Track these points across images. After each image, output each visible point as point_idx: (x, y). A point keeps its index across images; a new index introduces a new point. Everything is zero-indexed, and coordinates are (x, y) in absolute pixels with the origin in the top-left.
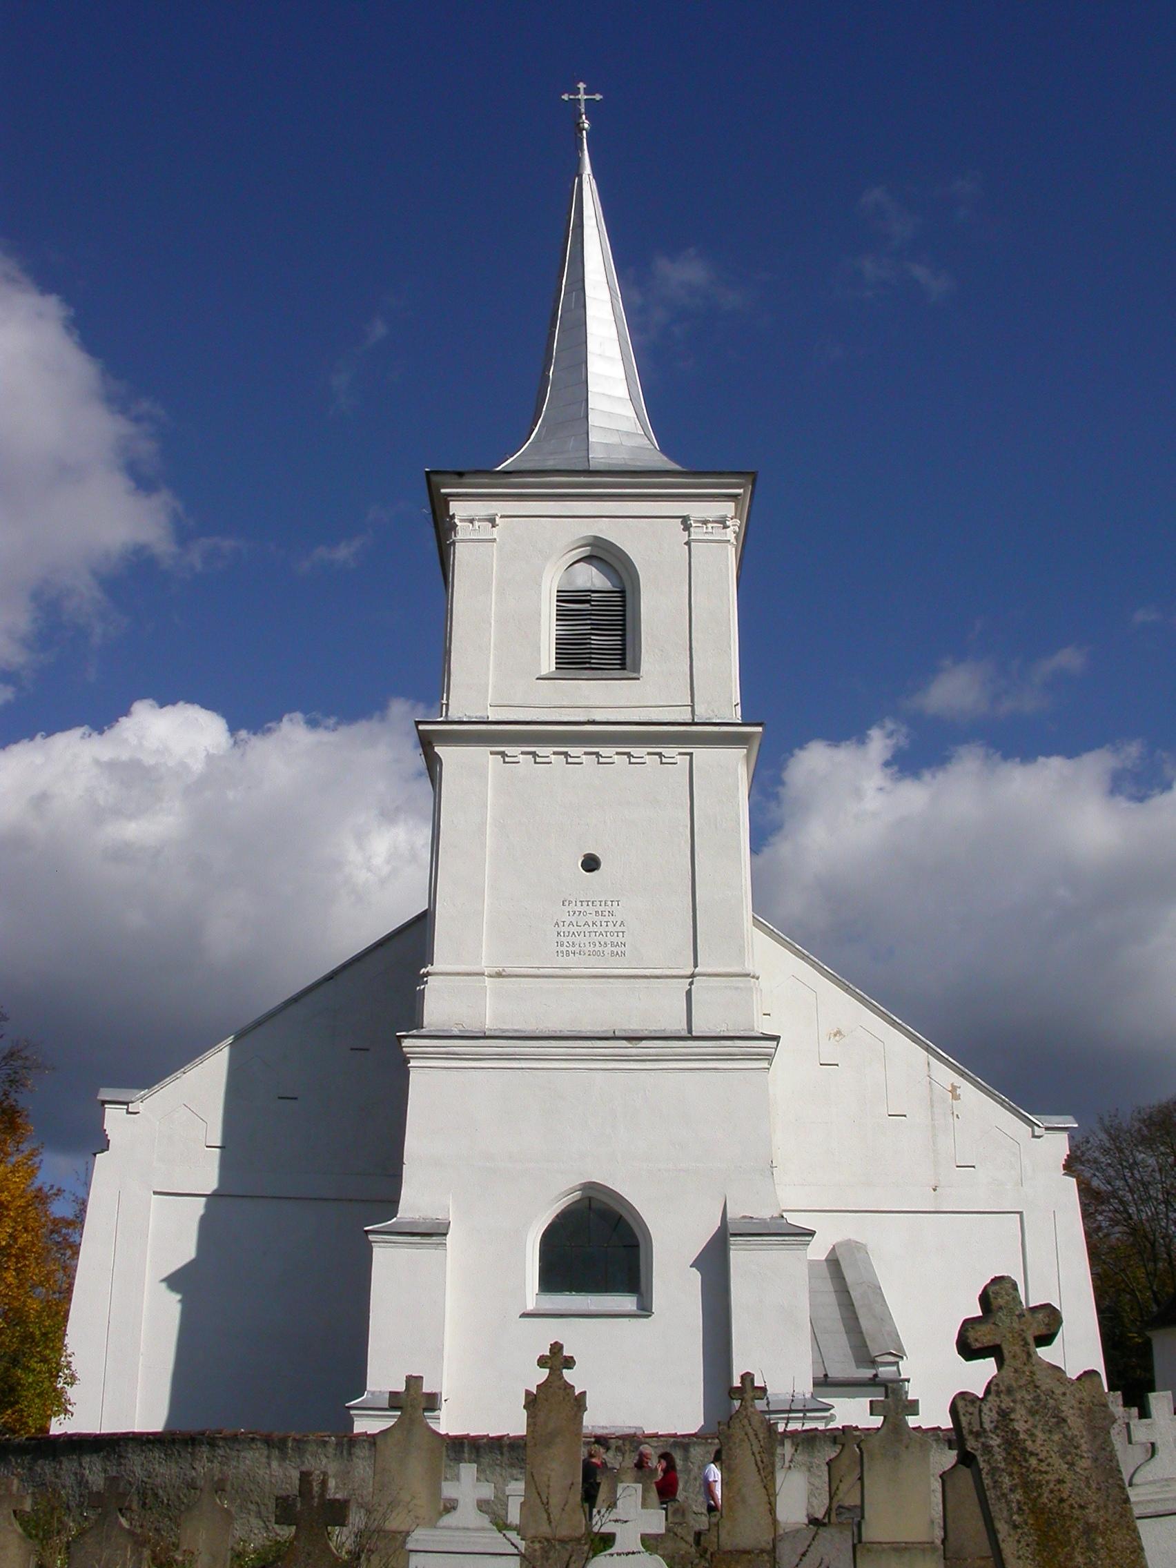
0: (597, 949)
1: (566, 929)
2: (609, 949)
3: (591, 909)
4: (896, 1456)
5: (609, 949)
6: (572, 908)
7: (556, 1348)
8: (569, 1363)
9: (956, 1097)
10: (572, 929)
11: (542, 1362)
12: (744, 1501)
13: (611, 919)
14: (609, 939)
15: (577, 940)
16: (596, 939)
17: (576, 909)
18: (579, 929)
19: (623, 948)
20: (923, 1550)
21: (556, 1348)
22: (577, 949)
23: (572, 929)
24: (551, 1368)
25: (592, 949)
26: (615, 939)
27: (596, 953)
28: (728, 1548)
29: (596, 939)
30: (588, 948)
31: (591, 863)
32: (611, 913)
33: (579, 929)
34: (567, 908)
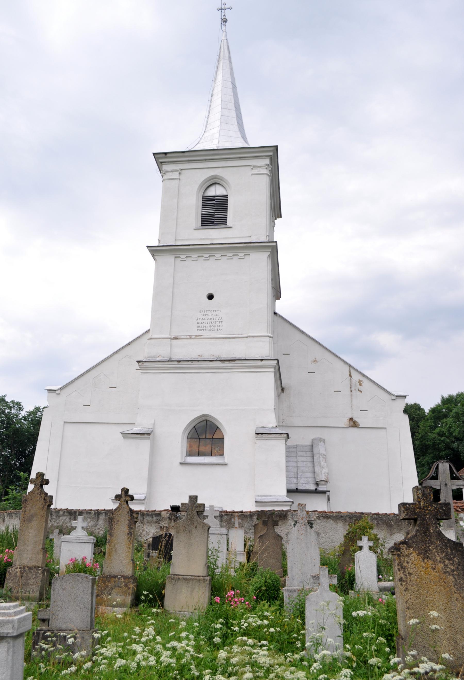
0: (212, 328)
1: (201, 321)
2: (216, 328)
3: (210, 313)
4: (190, 531)
5: (216, 328)
6: (203, 313)
7: (125, 491)
8: (47, 482)
9: (361, 385)
10: (203, 321)
11: (118, 497)
12: (116, 551)
13: (217, 317)
14: (216, 324)
15: (204, 325)
16: (212, 324)
17: (205, 314)
18: (205, 321)
19: (221, 328)
20: (199, 580)
21: (125, 491)
22: (204, 328)
23: (203, 321)
24: (35, 484)
25: (210, 328)
26: (219, 324)
27: (211, 330)
28: (106, 574)
29: (212, 324)
30: (208, 328)
31: (211, 297)
32: (218, 315)
33: (205, 321)
34: (201, 313)
